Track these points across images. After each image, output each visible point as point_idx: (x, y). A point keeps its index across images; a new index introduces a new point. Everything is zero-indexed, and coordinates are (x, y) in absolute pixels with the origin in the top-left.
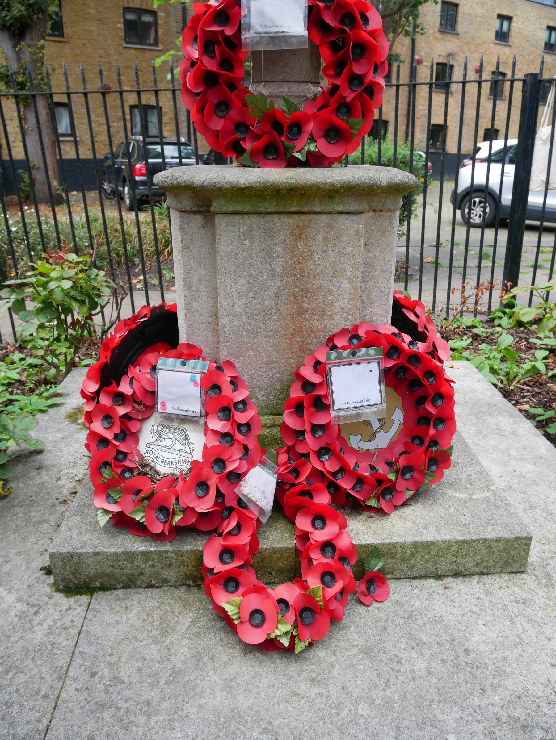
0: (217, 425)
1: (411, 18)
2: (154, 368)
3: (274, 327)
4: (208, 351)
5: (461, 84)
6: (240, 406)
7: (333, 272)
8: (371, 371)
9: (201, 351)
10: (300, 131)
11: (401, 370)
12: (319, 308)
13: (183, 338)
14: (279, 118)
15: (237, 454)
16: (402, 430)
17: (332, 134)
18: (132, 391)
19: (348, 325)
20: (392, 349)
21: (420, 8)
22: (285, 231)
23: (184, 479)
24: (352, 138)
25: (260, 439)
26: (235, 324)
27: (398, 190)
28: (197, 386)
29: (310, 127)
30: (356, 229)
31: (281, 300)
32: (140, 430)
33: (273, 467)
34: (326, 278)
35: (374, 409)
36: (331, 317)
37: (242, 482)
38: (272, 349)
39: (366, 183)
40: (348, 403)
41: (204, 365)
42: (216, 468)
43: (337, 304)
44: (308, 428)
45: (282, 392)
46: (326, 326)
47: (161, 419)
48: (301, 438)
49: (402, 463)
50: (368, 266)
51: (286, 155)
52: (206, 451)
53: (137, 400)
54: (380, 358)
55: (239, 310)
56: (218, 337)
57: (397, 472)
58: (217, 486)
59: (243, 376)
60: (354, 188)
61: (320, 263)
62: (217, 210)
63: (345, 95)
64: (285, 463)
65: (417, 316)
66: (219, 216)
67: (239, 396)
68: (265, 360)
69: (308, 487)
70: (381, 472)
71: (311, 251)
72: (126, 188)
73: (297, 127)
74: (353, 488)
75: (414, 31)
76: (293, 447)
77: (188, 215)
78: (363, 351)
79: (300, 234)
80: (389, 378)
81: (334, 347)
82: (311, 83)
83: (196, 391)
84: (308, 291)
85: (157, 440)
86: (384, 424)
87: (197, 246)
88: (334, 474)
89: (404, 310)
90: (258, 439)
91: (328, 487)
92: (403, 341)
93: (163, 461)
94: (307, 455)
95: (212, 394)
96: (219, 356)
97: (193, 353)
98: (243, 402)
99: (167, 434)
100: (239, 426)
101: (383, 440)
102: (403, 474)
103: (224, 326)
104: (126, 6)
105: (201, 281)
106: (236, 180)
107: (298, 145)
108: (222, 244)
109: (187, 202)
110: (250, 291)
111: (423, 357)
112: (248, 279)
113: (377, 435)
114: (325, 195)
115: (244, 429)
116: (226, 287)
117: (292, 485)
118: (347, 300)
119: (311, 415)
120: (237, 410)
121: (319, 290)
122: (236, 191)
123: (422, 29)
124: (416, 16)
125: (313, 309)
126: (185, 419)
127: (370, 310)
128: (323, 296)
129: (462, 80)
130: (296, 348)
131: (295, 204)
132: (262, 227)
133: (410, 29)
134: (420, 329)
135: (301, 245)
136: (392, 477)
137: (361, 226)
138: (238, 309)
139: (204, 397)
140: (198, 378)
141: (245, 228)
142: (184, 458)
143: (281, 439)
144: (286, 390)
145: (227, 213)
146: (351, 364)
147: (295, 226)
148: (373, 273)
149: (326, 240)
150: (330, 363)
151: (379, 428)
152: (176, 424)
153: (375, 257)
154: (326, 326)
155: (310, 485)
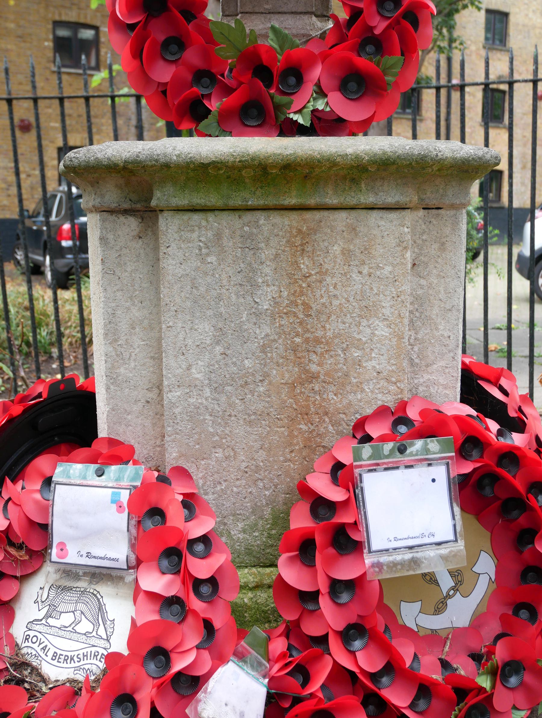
0: (156, 582)
1: (445, 31)
2: (48, 482)
3: (260, 406)
4: (145, 452)
5: (531, 85)
6: (200, 548)
7: (361, 308)
8: (434, 480)
9: (131, 450)
10: (300, 80)
11: (486, 481)
12: (337, 371)
13: (103, 430)
14: (265, 59)
15: (192, 638)
16: (495, 592)
17: (352, 86)
18: (6, 523)
19: (390, 401)
20: (469, 443)
21: (457, 17)
22: (276, 239)
23: (91, 691)
24: (386, 90)
25: (237, 611)
26: (192, 400)
27: (467, 171)
28: (123, 512)
29: (317, 72)
30: (397, 235)
31: (272, 358)
32: (16, 598)
33: (260, 664)
34: (348, 319)
35: (444, 551)
36: (359, 387)
37: (201, 695)
38: (257, 445)
39: (413, 155)
40: (396, 539)
41: (137, 473)
42: (152, 667)
43: (369, 365)
44: (323, 586)
45: (274, 524)
46: (350, 404)
47: (58, 576)
48: (311, 607)
49: (501, 654)
50: (420, 302)
51: (277, 118)
52: (136, 633)
53: (14, 541)
54: (449, 458)
55: (198, 376)
56: (163, 426)
57: (493, 673)
58: (152, 703)
59: (206, 494)
60: (394, 163)
61: (337, 293)
62: (163, 204)
63: (373, 24)
64: (283, 656)
65: (505, 393)
66: (165, 214)
67: (197, 529)
68: (244, 465)
69: (326, 704)
70: (463, 673)
71: (323, 273)
72: (48, 258)
73: (294, 73)
74: (412, 706)
75: (450, 46)
76: (296, 624)
77: (113, 217)
78: (419, 444)
79: (302, 245)
80: (474, 495)
81: (367, 439)
82: (317, 16)
83: (121, 521)
84: (318, 341)
85: (48, 616)
86: (461, 579)
87: (129, 269)
88: (374, 677)
89: (481, 382)
90: (233, 612)
91: (365, 704)
92: (488, 429)
93: (55, 655)
94: (323, 640)
95: (149, 525)
96: (163, 461)
97: (119, 453)
98: (205, 539)
99: (66, 602)
100: (197, 583)
101: (461, 612)
102: (505, 678)
103: (173, 405)
104: (57, 18)
105: (134, 328)
106: (194, 151)
107: (297, 102)
108: (171, 261)
109: (112, 196)
110: (218, 343)
111: (525, 456)
112: (214, 321)
113: (449, 602)
114: (344, 178)
115: (205, 589)
116: (176, 336)
117: (297, 700)
118: (385, 357)
119: (329, 562)
120: (193, 554)
121: (336, 341)
122: (194, 170)
123: (461, 44)
124: (451, 28)
125: (327, 374)
126: (101, 574)
127: (426, 377)
128: (344, 350)
129: (531, 77)
130: (298, 443)
131: (294, 193)
132: (238, 233)
133: (444, 44)
134: (512, 414)
135: (305, 264)
136: (484, 682)
137: (406, 230)
138: (197, 374)
139: (134, 531)
140: (125, 496)
141: (210, 234)
142: (94, 649)
143: (274, 611)
144: (281, 518)
145: (179, 210)
146: (397, 468)
147: (294, 231)
148: (428, 314)
149: (347, 254)
150: (360, 466)
151: (453, 588)
152: (82, 584)
153: (430, 286)
154: (350, 404)
155: (330, 699)
